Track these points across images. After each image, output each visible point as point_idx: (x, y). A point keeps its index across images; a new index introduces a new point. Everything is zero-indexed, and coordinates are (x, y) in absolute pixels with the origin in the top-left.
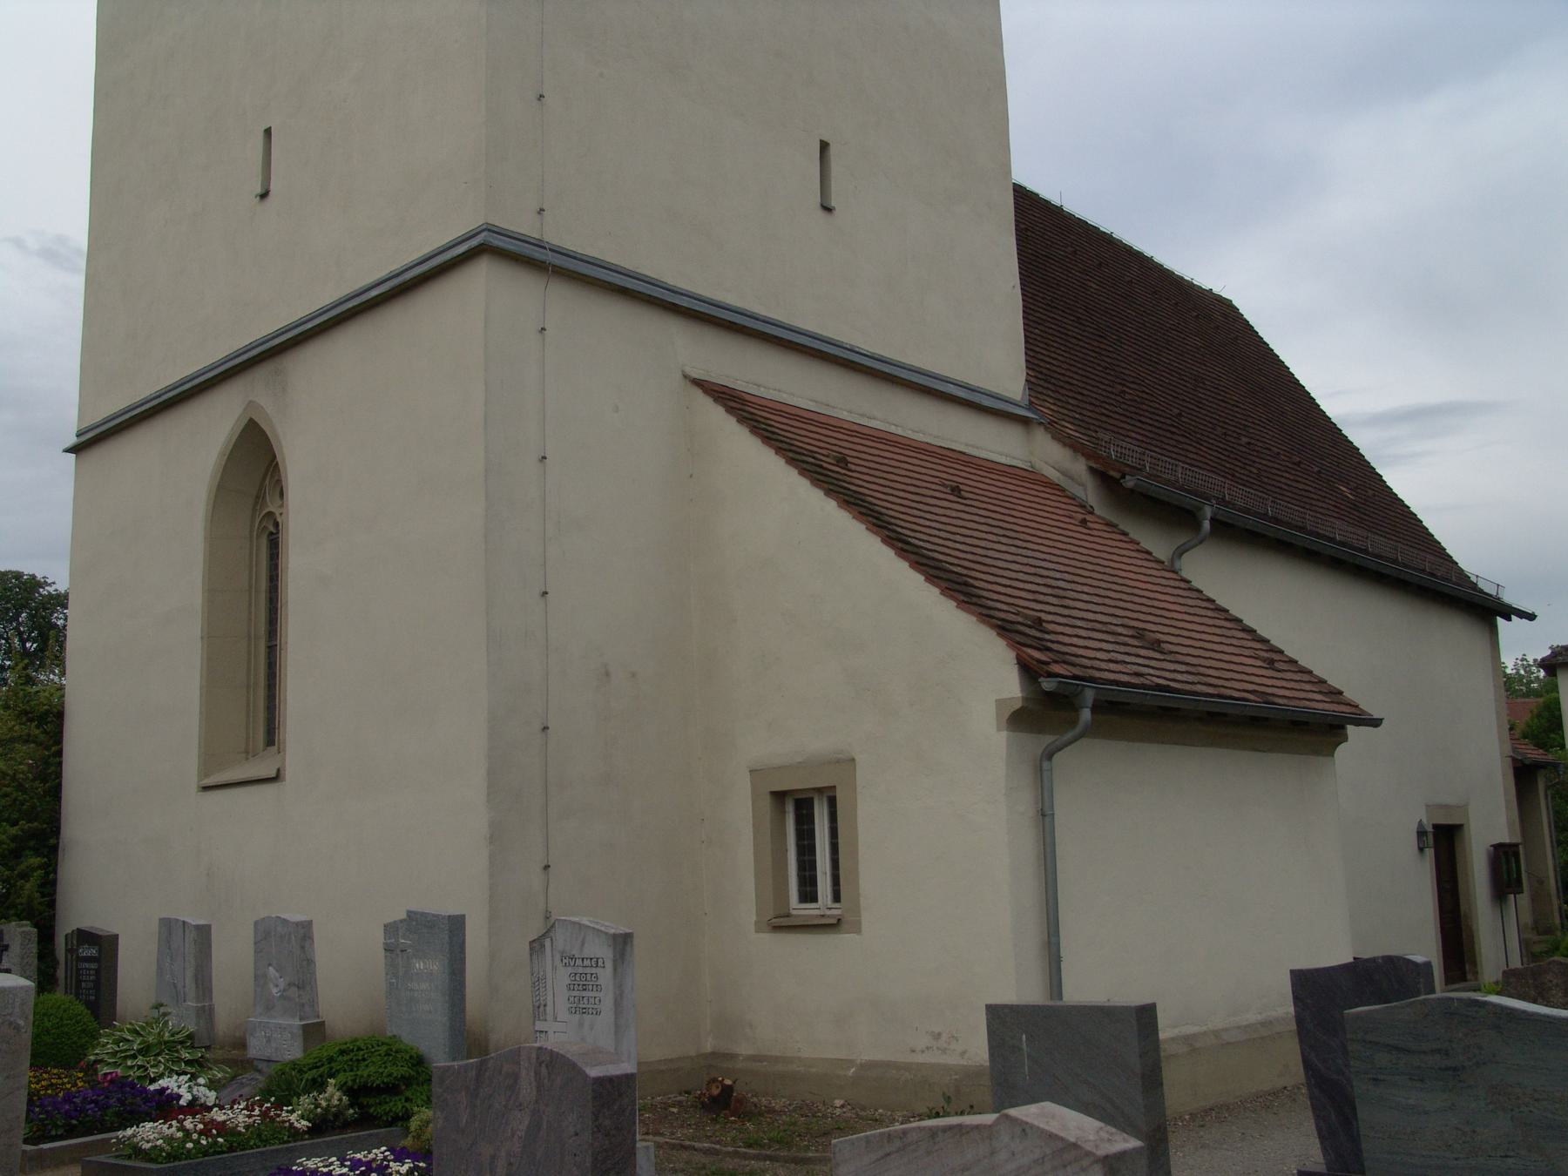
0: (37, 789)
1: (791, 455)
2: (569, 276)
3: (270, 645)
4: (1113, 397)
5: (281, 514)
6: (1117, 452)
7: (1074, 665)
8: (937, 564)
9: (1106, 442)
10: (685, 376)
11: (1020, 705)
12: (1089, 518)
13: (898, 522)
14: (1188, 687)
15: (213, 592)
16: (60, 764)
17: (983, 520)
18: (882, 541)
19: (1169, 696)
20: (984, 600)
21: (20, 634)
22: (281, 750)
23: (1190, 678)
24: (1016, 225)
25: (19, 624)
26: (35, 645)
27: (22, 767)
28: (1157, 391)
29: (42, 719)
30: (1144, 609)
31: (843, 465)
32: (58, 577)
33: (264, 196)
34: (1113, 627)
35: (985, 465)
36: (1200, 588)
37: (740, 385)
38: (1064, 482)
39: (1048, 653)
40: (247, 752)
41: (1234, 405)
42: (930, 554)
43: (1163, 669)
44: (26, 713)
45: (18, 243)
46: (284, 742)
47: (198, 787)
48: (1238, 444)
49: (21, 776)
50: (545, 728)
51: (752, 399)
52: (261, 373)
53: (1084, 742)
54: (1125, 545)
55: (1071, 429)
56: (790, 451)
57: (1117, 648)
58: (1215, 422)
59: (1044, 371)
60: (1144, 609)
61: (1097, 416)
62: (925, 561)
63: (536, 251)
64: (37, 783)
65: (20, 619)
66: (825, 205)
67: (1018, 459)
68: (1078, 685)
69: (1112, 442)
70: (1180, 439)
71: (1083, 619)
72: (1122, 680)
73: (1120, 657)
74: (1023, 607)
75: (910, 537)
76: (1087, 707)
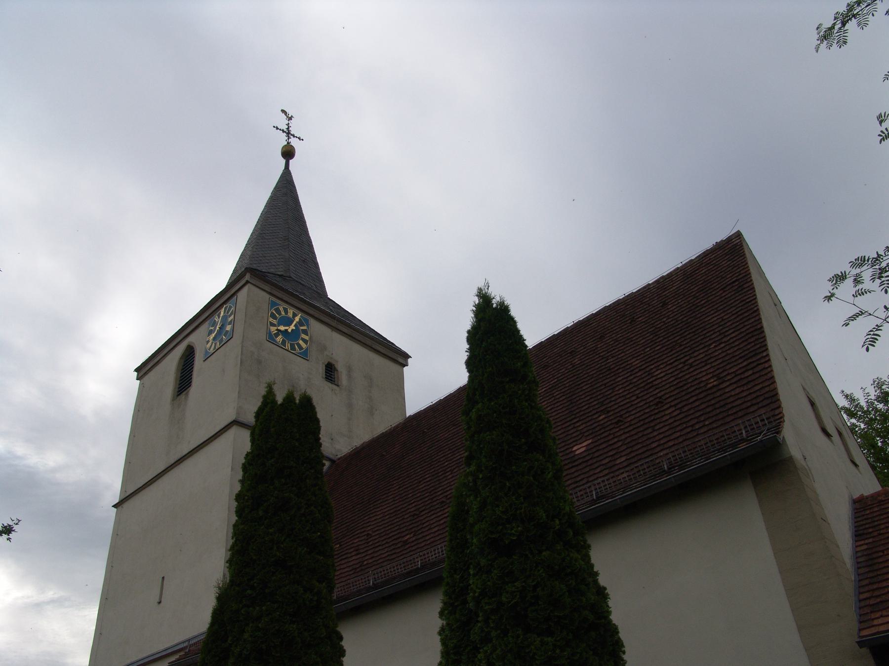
33: (160, 603)
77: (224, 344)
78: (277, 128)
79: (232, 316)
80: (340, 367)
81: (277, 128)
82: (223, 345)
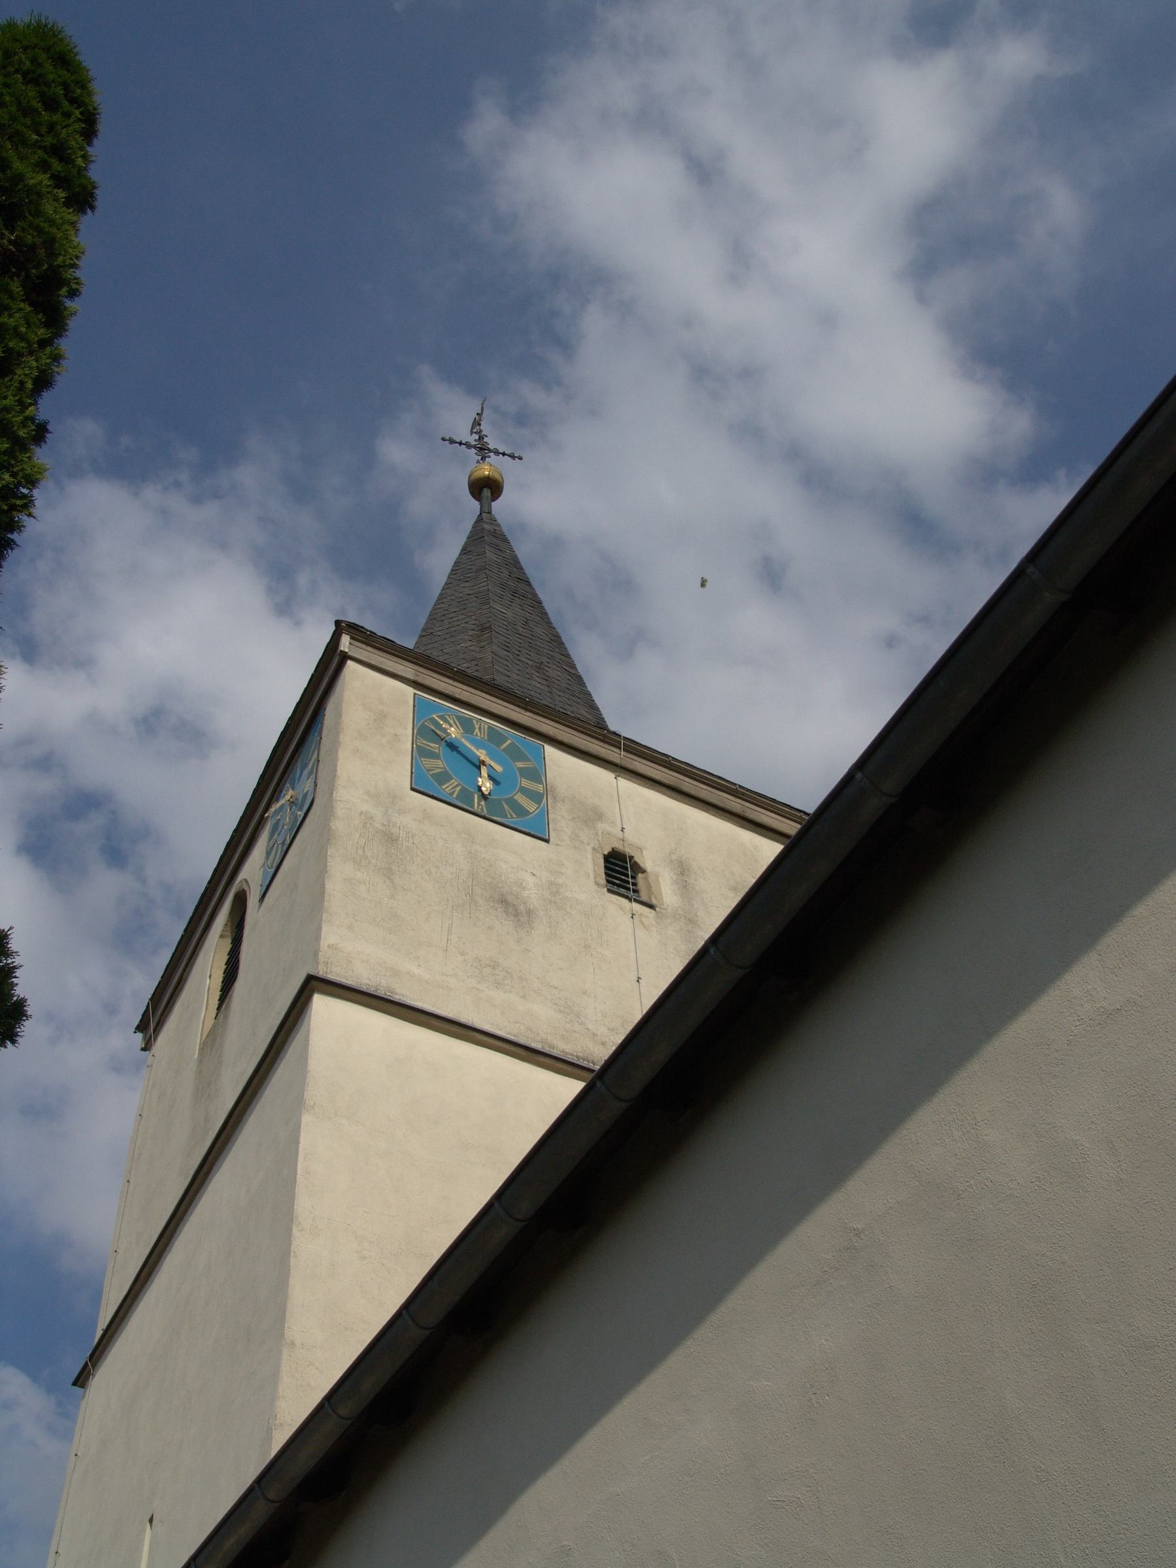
78: (452, 441)
80: (648, 860)
81: (452, 441)
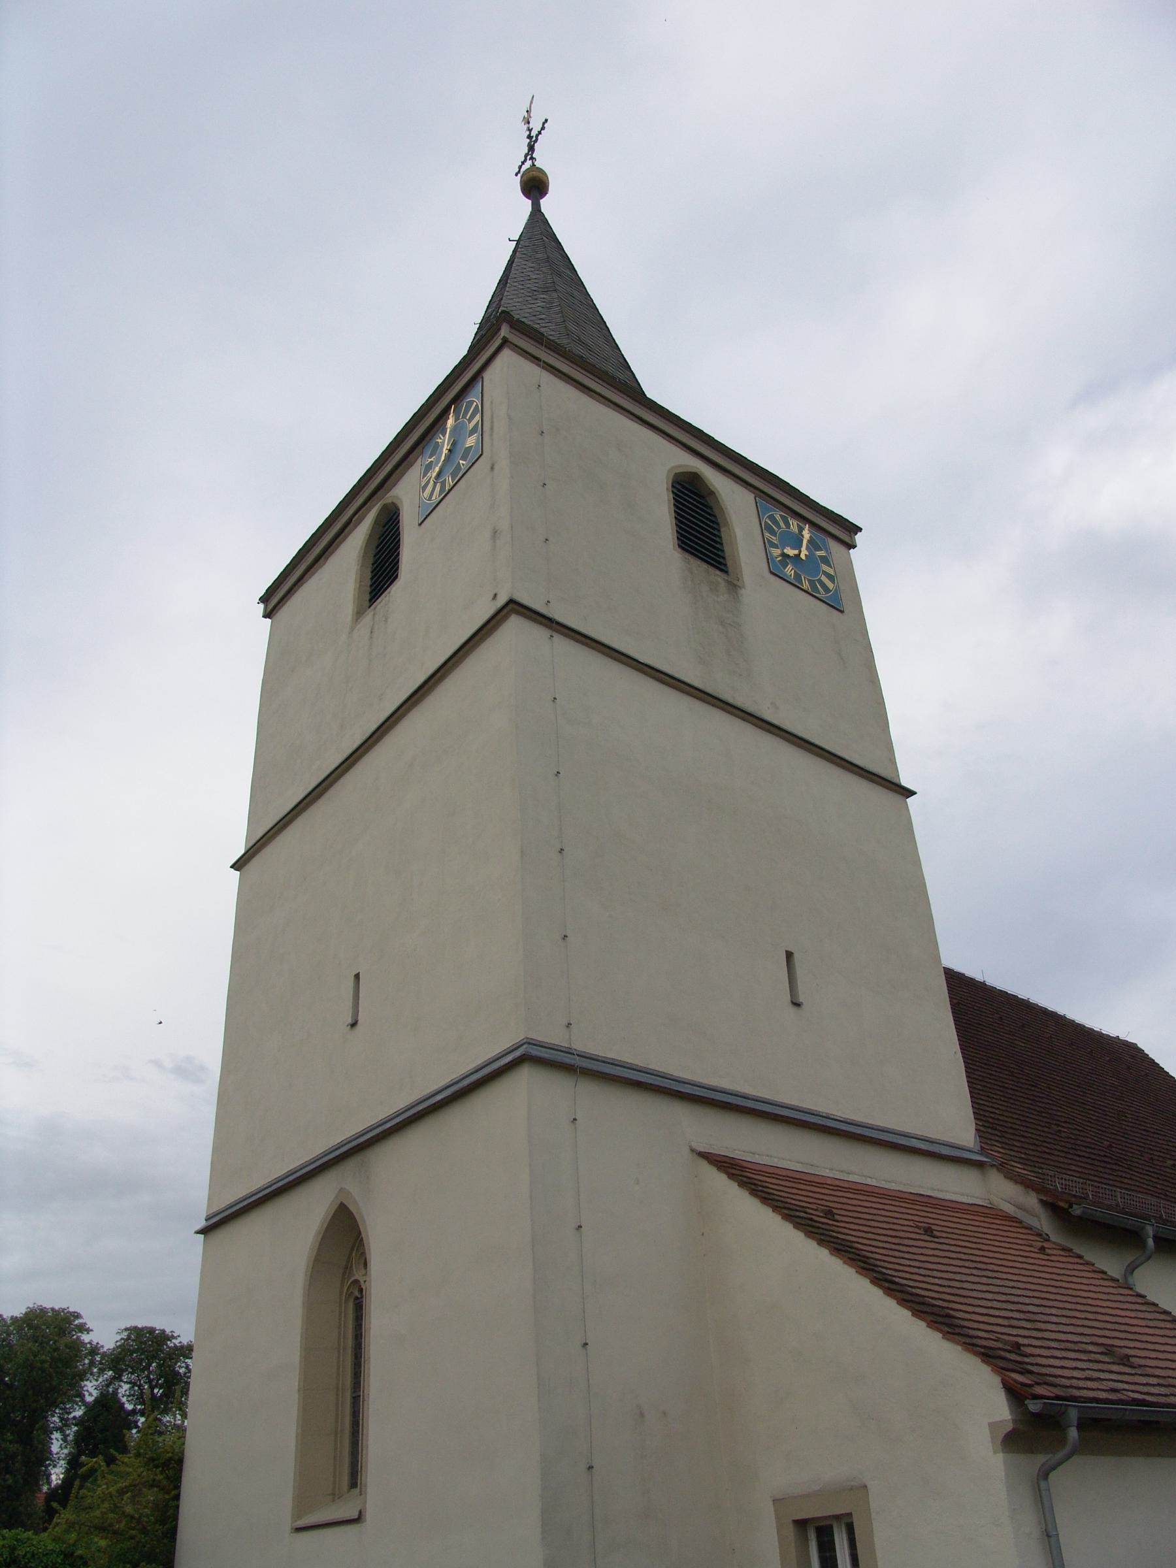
0: (157, 1531)
1: (786, 1212)
2: (603, 1078)
3: (354, 1396)
4: (1050, 1136)
5: (365, 1281)
6: (1062, 1184)
7: (1055, 1386)
8: (921, 1299)
9: (1051, 1176)
10: (692, 1150)
11: (1011, 1428)
12: (1046, 1245)
13: (882, 1264)
14: (1162, 1400)
15: (309, 1350)
16: (178, 1507)
17: (954, 1255)
18: (871, 1282)
19: (1147, 1410)
20: (967, 1330)
21: (150, 1381)
22: (363, 1493)
23: (1163, 1390)
24: (950, 1001)
25: (150, 1373)
26: (161, 1391)
27: (146, 1510)
28: (1086, 1128)
29: (166, 1464)
30: (1109, 1326)
31: (829, 1216)
32: (184, 1331)
33: (354, 1025)
34: (1084, 1346)
35: (949, 1205)
36: (1156, 1302)
37: (737, 1155)
38: (1019, 1214)
39: (1029, 1375)
40: (334, 1494)
41: (1154, 1133)
42: (914, 1290)
43: (1136, 1383)
44: (152, 1460)
45: (158, 1064)
46: (366, 1486)
47: (292, 1529)
48: (1164, 1167)
49: (145, 1519)
50: (590, 1468)
51: (749, 1165)
52: (351, 1164)
53: (1075, 1458)
54: (1081, 1267)
55: (1019, 1168)
56: (785, 1208)
57: (1091, 1365)
58: (1142, 1149)
59: (990, 1120)
60: (1109, 1326)
61: (1039, 1154)
62: (910, 1298)
63: (565, 1057)
64: (157, 1526)
65: (151, 1368)
66: (794, 1001)
67: (977, 1198)
68: (1061, 1405)
69: (1057, 1176)
70: (1114, 1167)
71: (1056, 1340)
72: (1101, 1397)
73: (1095, 1375)
74: (1002, 1334)
75: (894, 1276)
76: (1074, 1426)
77: (765, 546)
79: (478, 417)
82: (764, 543)
